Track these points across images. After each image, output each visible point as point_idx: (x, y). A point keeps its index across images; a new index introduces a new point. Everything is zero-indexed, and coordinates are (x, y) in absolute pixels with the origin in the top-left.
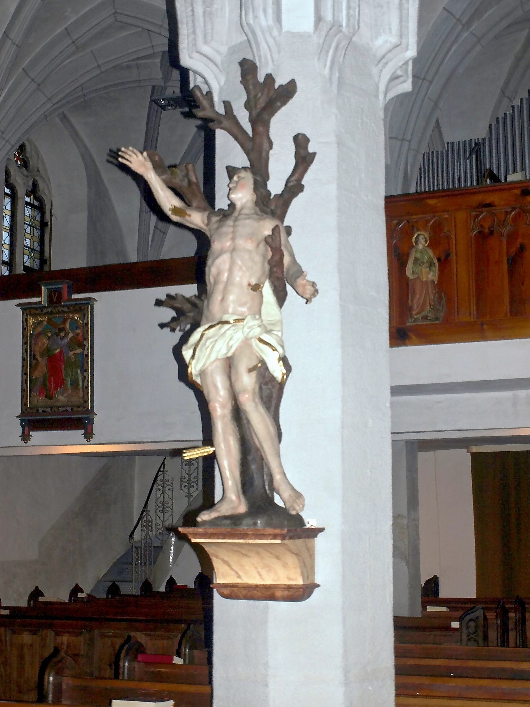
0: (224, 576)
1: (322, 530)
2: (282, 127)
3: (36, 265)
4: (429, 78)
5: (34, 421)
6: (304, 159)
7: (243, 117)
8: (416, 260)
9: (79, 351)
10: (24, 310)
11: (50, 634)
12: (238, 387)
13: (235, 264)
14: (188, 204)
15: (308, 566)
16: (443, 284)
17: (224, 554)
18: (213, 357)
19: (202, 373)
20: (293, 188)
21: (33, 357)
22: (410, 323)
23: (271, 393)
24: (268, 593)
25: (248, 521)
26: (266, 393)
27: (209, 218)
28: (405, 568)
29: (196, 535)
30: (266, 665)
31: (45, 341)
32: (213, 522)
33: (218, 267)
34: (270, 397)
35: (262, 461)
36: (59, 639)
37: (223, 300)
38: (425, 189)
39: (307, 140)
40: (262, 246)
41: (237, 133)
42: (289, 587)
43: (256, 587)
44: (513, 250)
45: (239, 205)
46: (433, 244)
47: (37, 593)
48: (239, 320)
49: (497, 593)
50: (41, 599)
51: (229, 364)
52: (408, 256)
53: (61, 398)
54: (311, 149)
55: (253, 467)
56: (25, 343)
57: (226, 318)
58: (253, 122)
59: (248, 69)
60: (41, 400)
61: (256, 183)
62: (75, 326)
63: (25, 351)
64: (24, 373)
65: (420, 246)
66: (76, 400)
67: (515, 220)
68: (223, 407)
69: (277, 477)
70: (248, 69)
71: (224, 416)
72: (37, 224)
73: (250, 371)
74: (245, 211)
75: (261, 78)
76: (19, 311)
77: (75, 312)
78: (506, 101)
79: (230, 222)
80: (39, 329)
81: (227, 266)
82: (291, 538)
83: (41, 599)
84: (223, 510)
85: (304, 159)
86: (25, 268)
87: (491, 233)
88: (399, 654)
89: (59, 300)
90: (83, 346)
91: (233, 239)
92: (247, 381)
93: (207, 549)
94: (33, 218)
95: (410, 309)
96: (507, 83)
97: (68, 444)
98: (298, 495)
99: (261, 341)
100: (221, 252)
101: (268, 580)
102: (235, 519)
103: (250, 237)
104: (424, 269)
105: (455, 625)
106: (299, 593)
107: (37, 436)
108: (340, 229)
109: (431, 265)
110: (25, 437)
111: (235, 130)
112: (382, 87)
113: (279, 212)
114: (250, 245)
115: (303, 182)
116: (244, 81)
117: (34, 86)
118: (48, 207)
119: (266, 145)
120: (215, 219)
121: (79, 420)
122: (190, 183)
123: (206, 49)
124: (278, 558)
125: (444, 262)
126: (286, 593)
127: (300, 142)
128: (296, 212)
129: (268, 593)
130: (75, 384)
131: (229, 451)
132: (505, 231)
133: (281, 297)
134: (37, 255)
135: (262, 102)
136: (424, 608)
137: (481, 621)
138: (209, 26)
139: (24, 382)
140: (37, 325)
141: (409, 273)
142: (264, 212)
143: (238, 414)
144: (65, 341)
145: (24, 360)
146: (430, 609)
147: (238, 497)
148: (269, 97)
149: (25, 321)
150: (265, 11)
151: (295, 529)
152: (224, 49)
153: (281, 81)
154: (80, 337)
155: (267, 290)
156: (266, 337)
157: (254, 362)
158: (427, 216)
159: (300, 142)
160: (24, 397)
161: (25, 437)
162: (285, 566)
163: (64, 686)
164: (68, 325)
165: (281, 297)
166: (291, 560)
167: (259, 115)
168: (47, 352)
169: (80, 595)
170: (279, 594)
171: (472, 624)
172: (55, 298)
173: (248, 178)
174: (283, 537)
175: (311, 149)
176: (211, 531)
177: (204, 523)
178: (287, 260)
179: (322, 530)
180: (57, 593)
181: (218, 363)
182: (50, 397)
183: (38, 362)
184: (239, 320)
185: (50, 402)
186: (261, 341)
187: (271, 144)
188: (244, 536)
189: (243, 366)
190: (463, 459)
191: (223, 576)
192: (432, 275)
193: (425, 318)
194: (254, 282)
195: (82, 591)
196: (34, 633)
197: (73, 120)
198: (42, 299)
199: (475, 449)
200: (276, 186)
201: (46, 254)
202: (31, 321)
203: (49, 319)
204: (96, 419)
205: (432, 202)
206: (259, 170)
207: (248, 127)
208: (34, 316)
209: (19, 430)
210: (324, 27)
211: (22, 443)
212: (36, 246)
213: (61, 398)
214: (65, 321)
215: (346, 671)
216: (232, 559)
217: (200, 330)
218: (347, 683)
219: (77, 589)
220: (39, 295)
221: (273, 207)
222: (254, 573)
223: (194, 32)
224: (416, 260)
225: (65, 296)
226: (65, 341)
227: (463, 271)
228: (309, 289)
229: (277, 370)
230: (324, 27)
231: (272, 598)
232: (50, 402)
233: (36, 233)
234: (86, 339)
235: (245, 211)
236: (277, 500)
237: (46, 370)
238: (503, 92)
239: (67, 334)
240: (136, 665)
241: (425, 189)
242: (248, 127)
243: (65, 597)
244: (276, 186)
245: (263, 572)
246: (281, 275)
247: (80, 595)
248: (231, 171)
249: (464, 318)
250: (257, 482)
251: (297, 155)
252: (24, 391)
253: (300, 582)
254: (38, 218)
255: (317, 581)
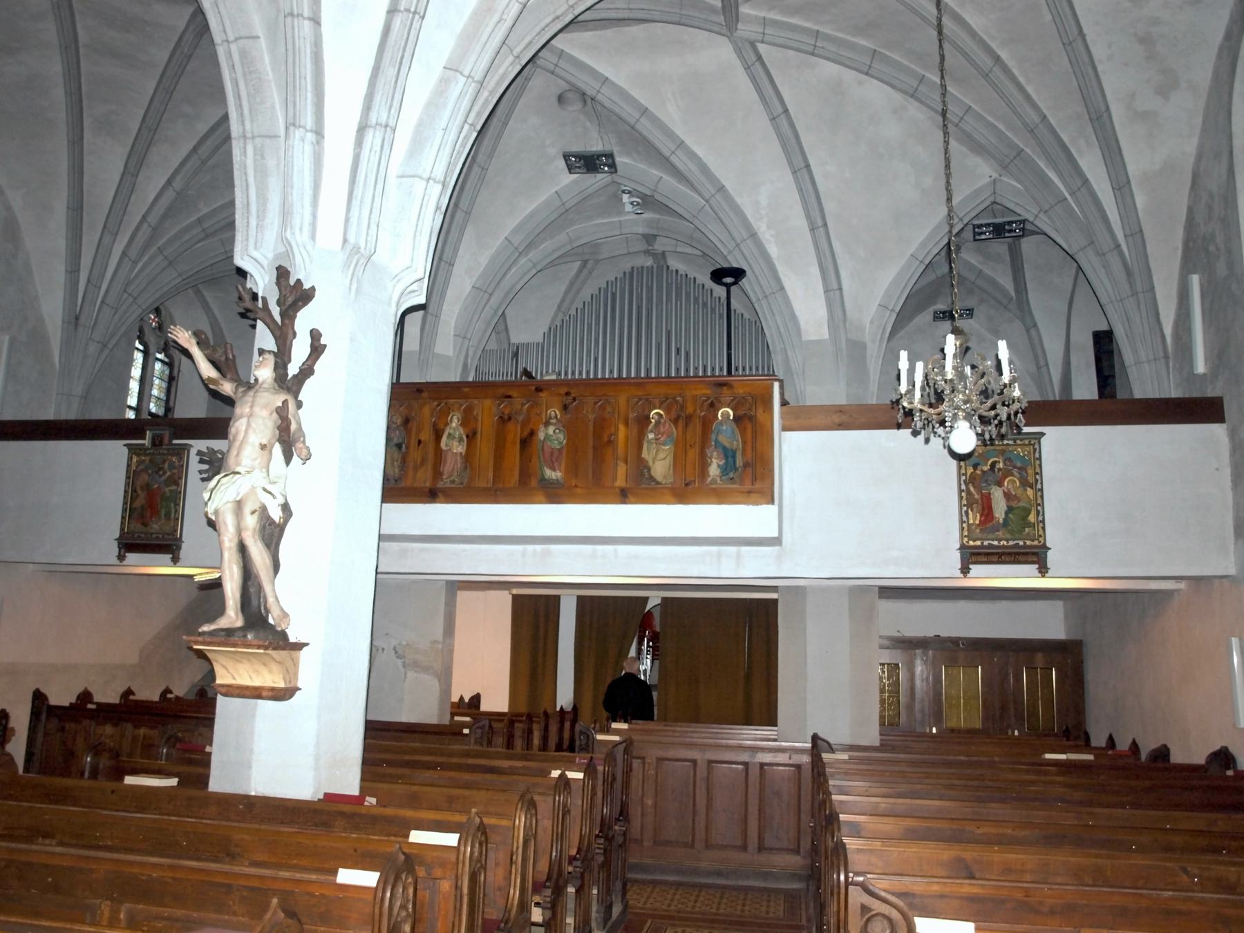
0: (222, 677)
1: (307, 644)
2: (304, 321)
3: (161, 412)
4: (490, 291)
5: (128, 545)
6: (317, 349)
7: (276, 311)
8: (450, 434)
9: (174, 488)
10: (129, 450)
11: (129, 726)
12: (243, 524)
13: (253, 426)
14: (224, 375)
15: (291, 671)
16: (468, 458)
17: (221, 659)
18: (224, 501)
19: (216, 512)
20: (307, 371)
21: (134, 491)
22: (440, 485)
23: (272, 533)
24: (256, 693)
25: (240, 634)
26: (267, 532)
27: (237, 388)
28: (437, 684)
29: (197, 643)
30: (251, 751)
31: (146, 477)
32: (211, 633)
33: (239, 427)
34: (272, 535)
35: (260, 588)
36: (137, 731)
37: (238, 455)
38: (648, 371)
39: (320, 335)
40: (275, 415)
41: (271, 323)
42: (273, 689)
43: (247, 688)
44: (526, 434)
45: (260, 381)
46: (464, 423)
47: (129, 692)
48: (248, 472)
49: (523, 708)
50: (132, 697)
51: (239, 505)
52: (443, 431)
53: (155, 526)
54: (323, 342)
55: (252, 590)
56: (128, 478)
57: (238, 469)
58: (282, 315)
59: (282, 274)
60: (137, 527)
61: (276, 364)
62: (172, 466)
63: (127, 484)
64: (125, 503)
65: (454, 425)
66: (167, 529)
67: (528, 410)
68: (230, 541)
69: (271, 600)
70: (282, 274)
71: (230, 548)
72: (166, 378)
73: (253, 513)
74: (265, 386)
75: (292, 282)
76: (126, 450)
77: (173, 455)
78: (561, 314)
79: (251, 393)
80: (142, 467)
81: (244, 428)
82: (275, 649)
83: (132, 697)
84: (223, 623)
85: (317, 349)
86: (150, 414)
87: (510, 419)
88: (367, 749)
89: (161, 444)
90: (177, 484)
91: (251, 407)
92: (251, 522)
93: (209, 655)
94: (163, 372)
95: (441, 474)
96: (563, 300)
97: (161, 567)
98: (286, 615)
99: (265, 490)
100: (241, 417)
101: (257, 682)
102: (229, 632)
103: (265, 406)
104: (456, 443)
105: (466, 731)
106: (283, 694)
107: (132, 557)
108: (348, 406)
109: (461, 440)
110: (121, 557)
111: (268, 320)
112: (395, 299)
113: (294, 388)
114: (265, 413)
115: (315, 368)
116: (278, 283)
117: (166, 263)
118: (176, 364)
119: (290, 336)
120: (241, 389)
121: (169, 546)
122: (227, 358)
123: (255, 254)
124: (265, 664)
125: (471, 437)
126: (270, 694)
127: (315, 335)
128: (308, 391)
129: (256, 693)
130: (168, 516)
131: (232, 576)
132: (520, 419)
133: (288, 458)
134: (163, 404)
135: (290, 300)
136: (452, 717)
137: (487, 729)
138: (260, 235)
139: (124, 510)
140: (140, 463)
141: (443, 445)
142: (281, 387)
143: (242, 549)
144: (164, 478)
145: (126, 492)
146: (457, 718)
147: (237, 614)
148: (297, 297)
149: (130, 459)
150: (301, 229)
151: (279, 642)
152: (271, 256)
153: (307, 286)
154: (176, 477)
155: (277, 449)
156: (269, 488)
157: (257, 506)
158: (461, 401)
159: (315, 335)
160: (122, 523)
161: (121, 557)
162: (271, 671)
163: (101, 766)
164: (166, 466)
165: (288, 458)
166: (274, 667)
167: (286, 310)
168: (147, 487)
169: (169, 696)
170: (265, 694)
171: (479, 731)
172: (157, 442)
173: (271, 360)
174: (266, 648)
175: (323, 342)
176: (208, 639)
177: (204, 633)
178: (293, 427)
179: (307, 644)
180: (150, 693)
181: (230, 506)
182: (144, 524)
183: (138, 496)
184: (248, 472)
185: (144, 529)
186: (265, 490)
187: (295, 334)
188: (234, 646)
189: (247, 510)
190: (503, 602)
191: (222, 678)
192: (459, 448)
193: (453, 482)
194: (264, 442)
195: (171, 692)
196: (115, 725)
197: (206, 293)
198: (146, 442)
199: (515, 591)
200: (293, 369)
201: (171, 404)
202: (135, 459)
203: (151, 461)
204: (184, 546)
205: (466, 390)
206: (282, 357)
207: (278, 319)
208: (138, 455)
209: (116, 551)
210: (349, 248)
211: (118, 562)
212: (163, 396)
213: (155, 527)
214: (164, 462)
215: (317, 758)
216: (230, 664)
217: (218, 477)
218: (317, 769)
219: (168, 691)
220: (144, 439)
221: (290, 385)
222: (246, 675)
223: (247, 240)
224: (450, 434)
225: (166, 440)
226: (164, 478)
227: (485, 449)
228: (305, 452)
229: (276, 514)
230: (349, 248)
231: (260, 697)
232: (144, 529)
233: (164, 385)
234: (180, 478)
235: (265, 386)
236: (271, 621)
237: (144, 502)
238: (559, 307)
239: (165, 473)
240: (174, 751)
241: (648, 371)
242: (278, 319)
243: (156, 698)
244: (293, 369)
245: (254, 676)
246: (288, 439)
247: (169, 696)
248: (261, 352)
249: (482, 484)
250: (254, 602)
251: (312, 346)
252: (123, 518)
253: (282, 685)
254: (167, 372)
255: (299, 685)
